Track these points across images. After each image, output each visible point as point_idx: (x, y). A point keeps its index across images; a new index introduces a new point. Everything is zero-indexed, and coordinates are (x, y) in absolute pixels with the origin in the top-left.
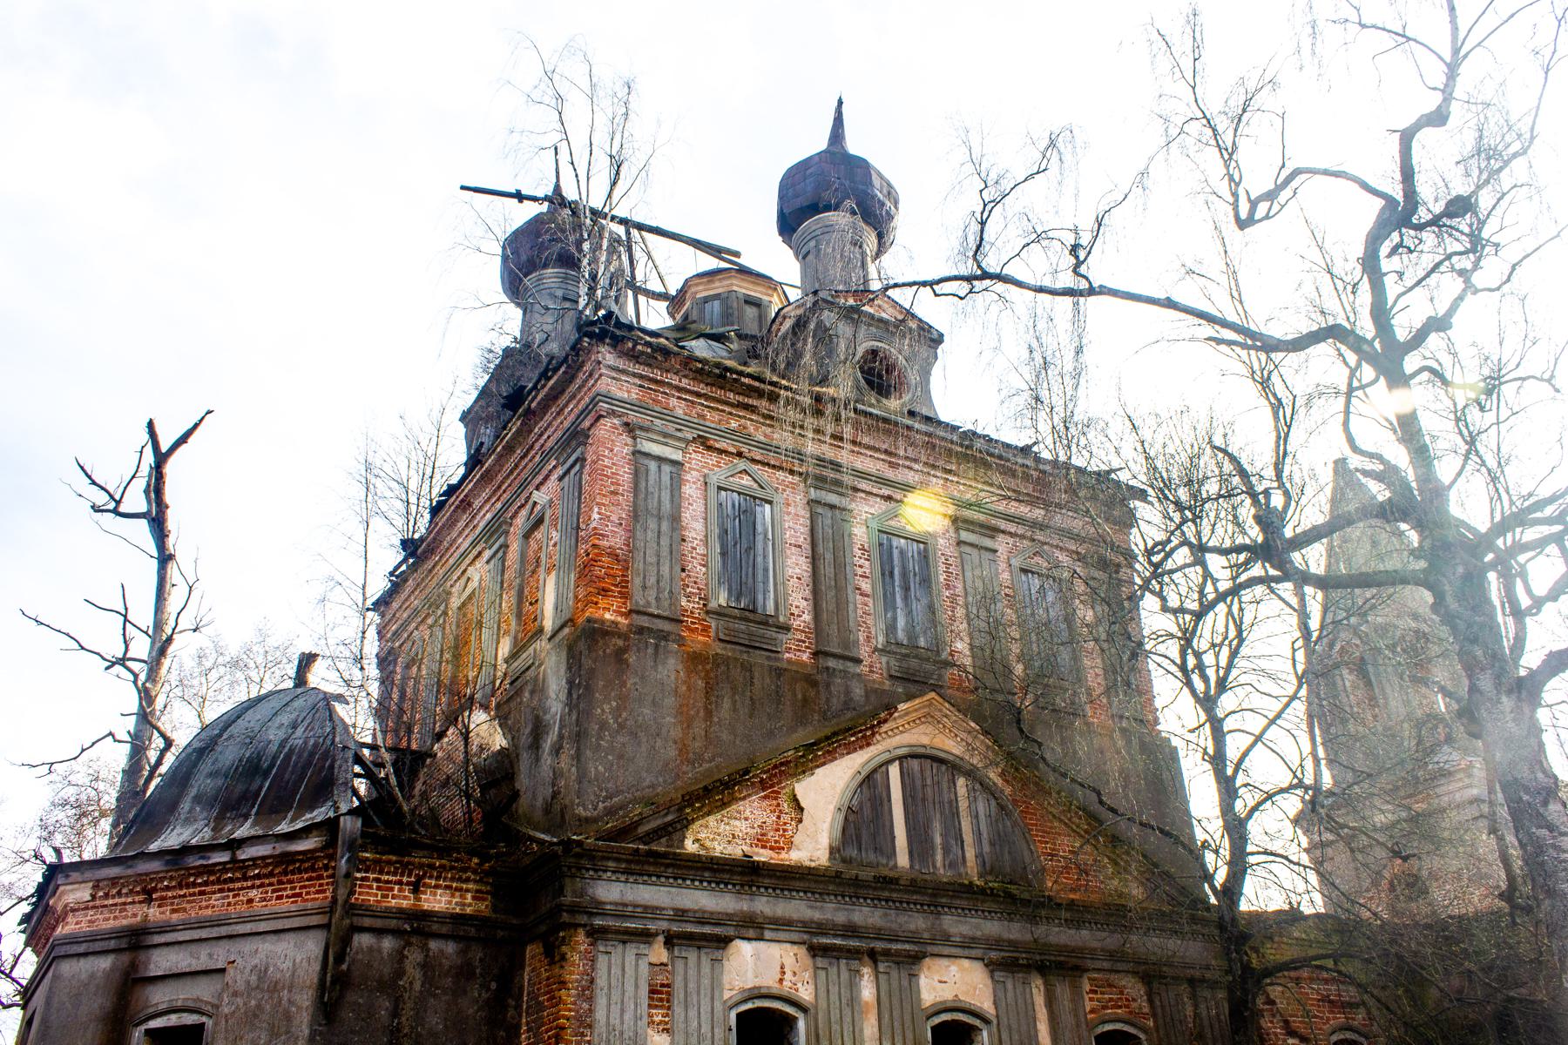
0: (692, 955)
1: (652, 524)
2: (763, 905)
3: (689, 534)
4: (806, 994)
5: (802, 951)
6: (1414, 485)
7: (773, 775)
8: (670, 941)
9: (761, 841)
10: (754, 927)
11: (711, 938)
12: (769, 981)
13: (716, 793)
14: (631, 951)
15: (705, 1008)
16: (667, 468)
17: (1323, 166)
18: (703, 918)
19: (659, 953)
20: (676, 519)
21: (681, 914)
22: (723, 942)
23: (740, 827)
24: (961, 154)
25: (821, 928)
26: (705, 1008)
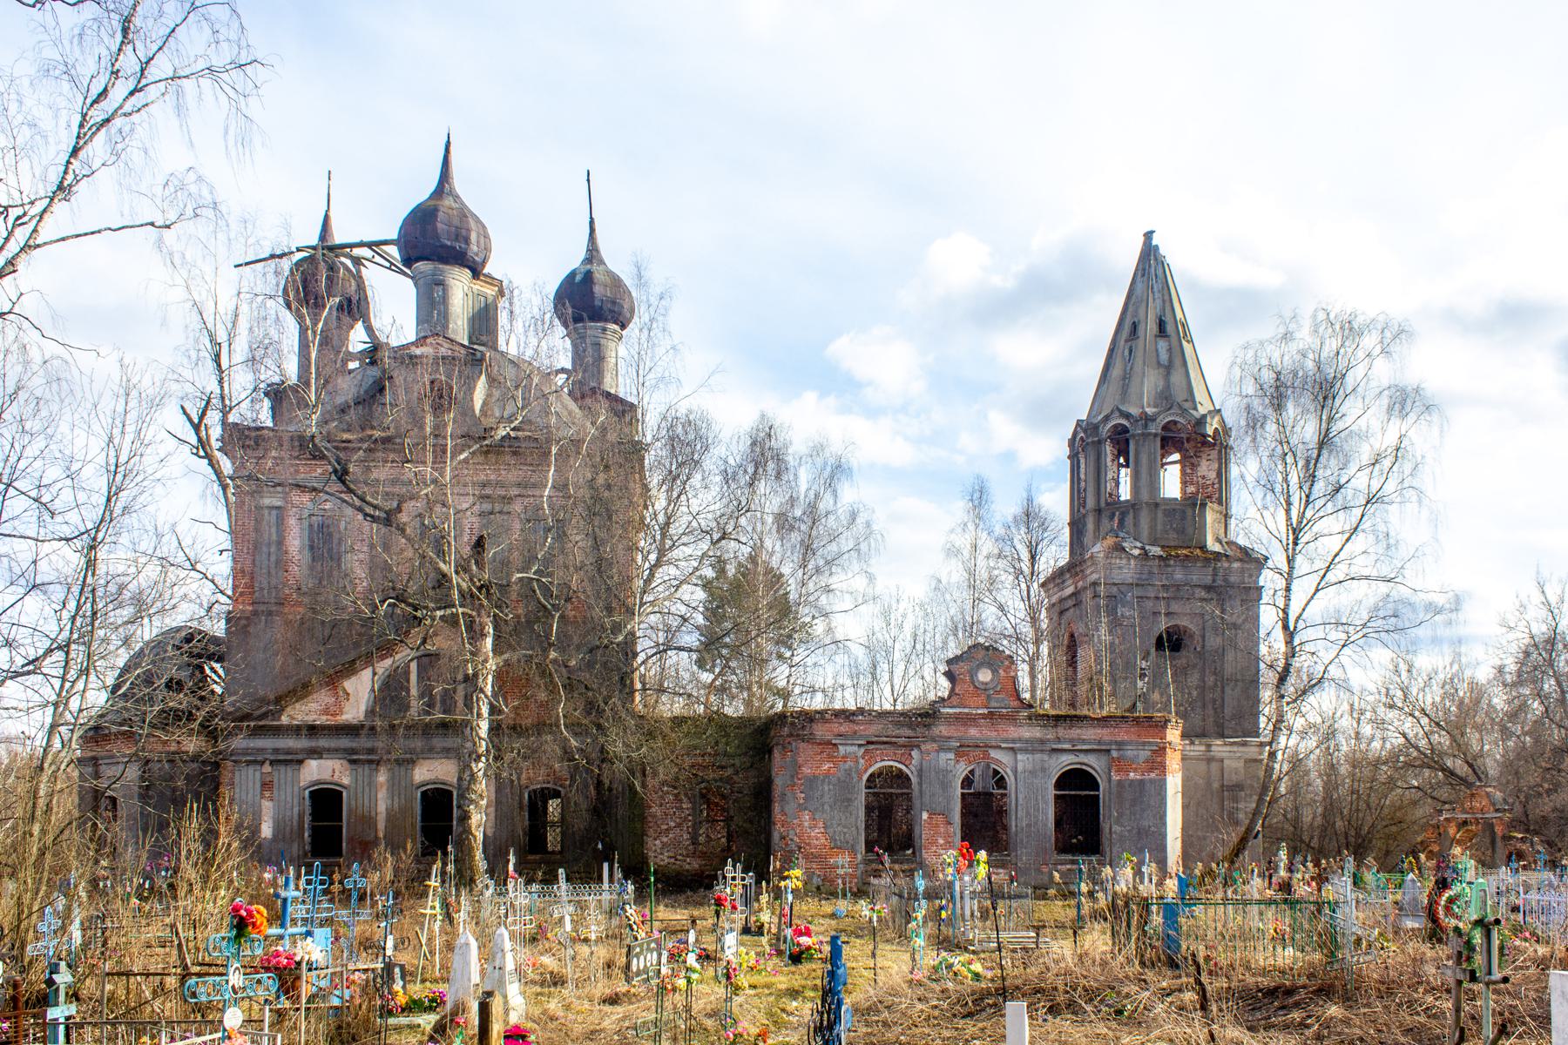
0: (282, 768)
1: (265, 549)
2: (323, 742)
3: (291, 549)
4: (346, 781)
5: (345, 762)
6: (381, 825)
7: (334, 678)
8: (272, 763)
9: (326, 712)
10: (316, 753)
11: (295, 761)
12: (326, 776)
13: (302, 691)
14: (251, 769)
15: (289, 790)
16: (274, 512)
17: (357, 240)
18: (288, 752)
19: (267, 768)
20: (281, 542)
21: (276, 751)
22: (301, 762)
23: (313, 706)
24: (1025, 495)
25: (353, 751)
26: (289, 790)
